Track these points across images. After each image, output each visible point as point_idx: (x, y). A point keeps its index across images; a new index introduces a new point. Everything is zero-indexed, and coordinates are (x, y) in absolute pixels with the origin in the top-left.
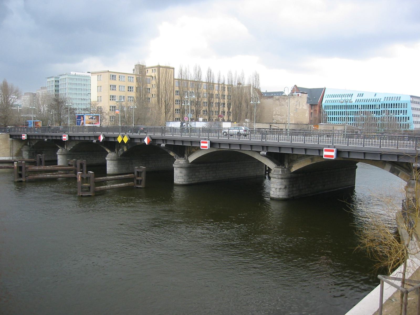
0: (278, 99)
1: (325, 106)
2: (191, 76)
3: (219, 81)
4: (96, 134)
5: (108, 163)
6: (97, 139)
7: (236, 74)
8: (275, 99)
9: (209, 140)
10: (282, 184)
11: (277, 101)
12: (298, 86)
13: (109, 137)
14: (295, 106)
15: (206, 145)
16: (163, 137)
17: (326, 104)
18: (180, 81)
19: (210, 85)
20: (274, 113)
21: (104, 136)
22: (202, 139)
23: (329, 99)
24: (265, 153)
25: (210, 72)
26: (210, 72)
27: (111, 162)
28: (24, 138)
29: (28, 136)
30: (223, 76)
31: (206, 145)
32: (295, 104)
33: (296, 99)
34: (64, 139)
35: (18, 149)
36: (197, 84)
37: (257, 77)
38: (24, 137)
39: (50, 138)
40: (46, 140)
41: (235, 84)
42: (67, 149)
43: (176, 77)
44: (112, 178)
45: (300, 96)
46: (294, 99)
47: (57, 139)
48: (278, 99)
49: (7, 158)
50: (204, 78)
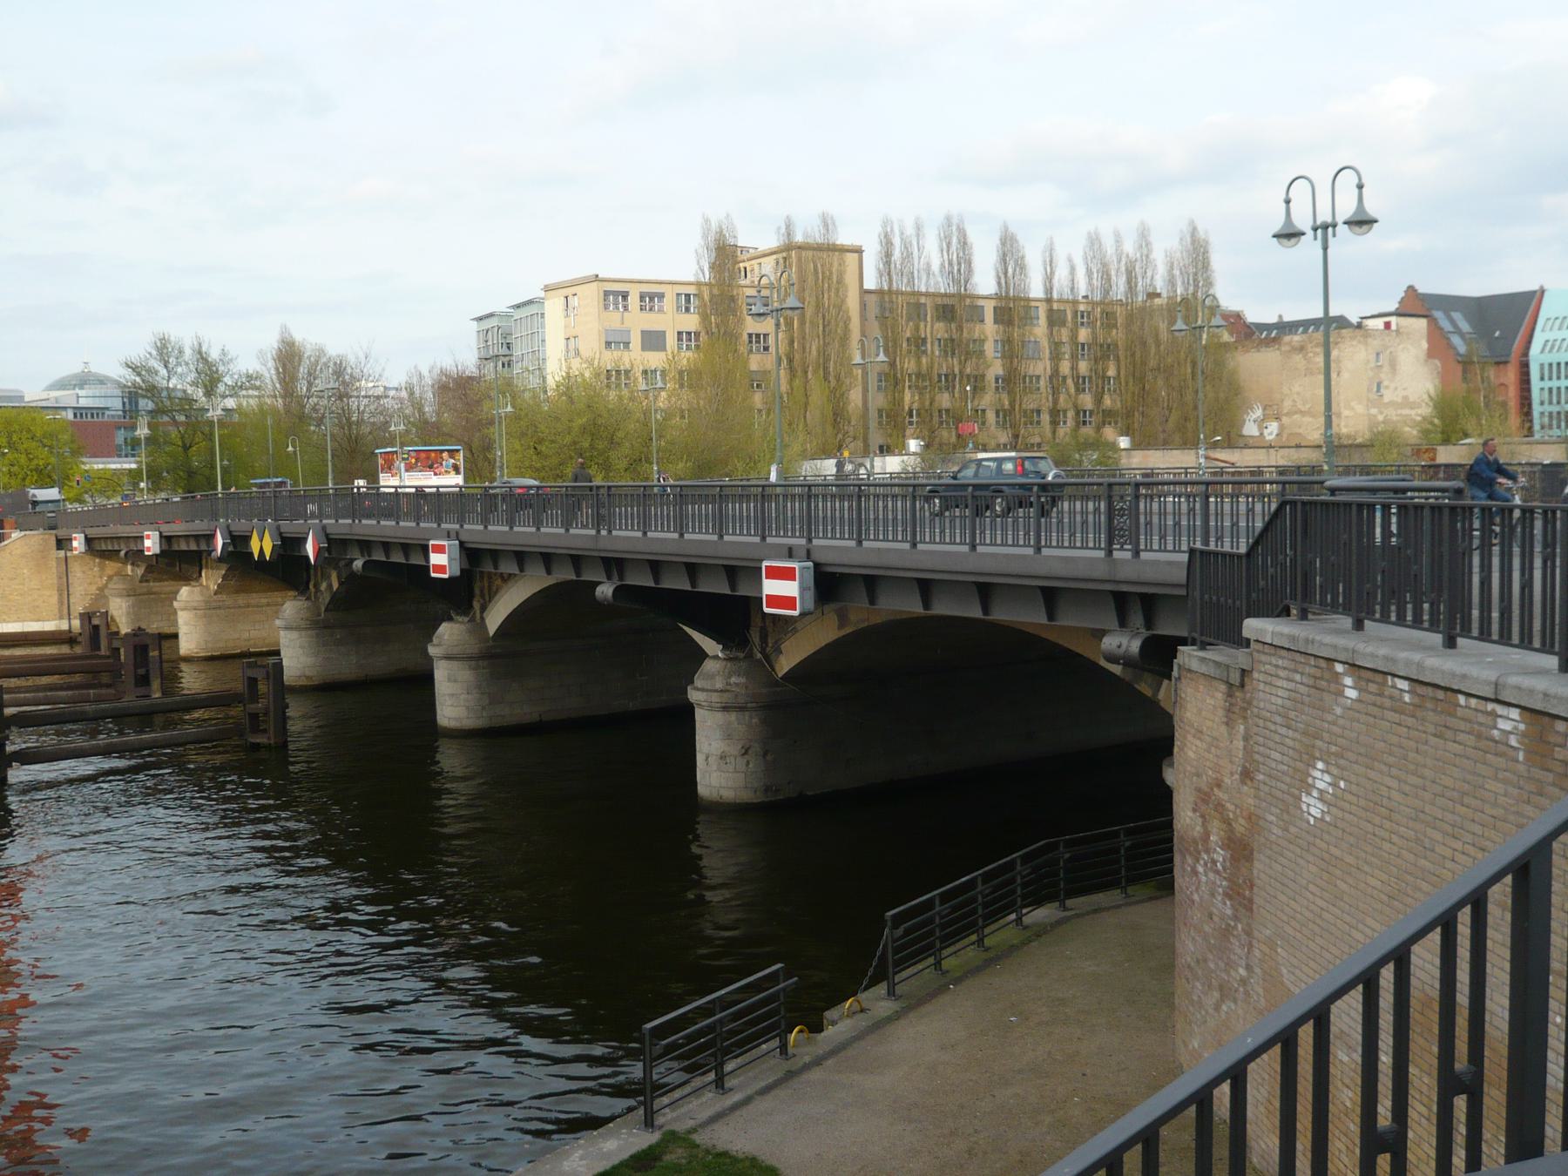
0: (1302, 349)
1: (1542, 365)
2: (932, 277)
3: (1049, 290)
4: (362, 531)
5: (443, 675)
6: (621, 579)
7: (1050, 264)
8: (1287, 348)
9: (808, 557)
10: (728, 737)
11: (1298, 358)
12: (1421, 290)
13: (496, 551)
14: (1371, 374)
15: (789, 588)
16: (1125, 573)
17: (1548, 358)
18: (884, 297)
19: (1011, 309)
20: (1287, 404)
21: (327, 535)
22: (777, 552)
23: (1551, 336)
24: (1135, 646)
25: (1009, 251)
26: (1009, 251)
27: (720, 717)
28: (441, 569)
29: (166, 539)
30: (1070, 260)
31: (789, 588)
32: (1372, 365)
33: (1375, 343)
34: (775, 601)
35: (93, 589)
36: (954, 309)
37: (1198, 255)
38: (151, 544)
39: (379, 556)
40: (605, 590)
41: (182, 381)
42: (207, 587)
43: (870, 283)
44: (23, 659)
45: (1394, 327)
46: (1366, 344)
47: (667, 584)
48: (1302, 349)
49: (49, 626)
50: (985, 282)
